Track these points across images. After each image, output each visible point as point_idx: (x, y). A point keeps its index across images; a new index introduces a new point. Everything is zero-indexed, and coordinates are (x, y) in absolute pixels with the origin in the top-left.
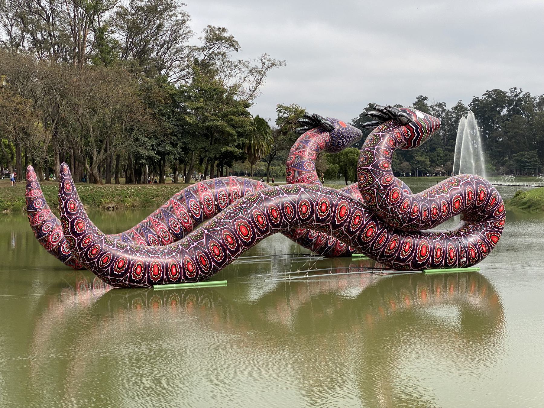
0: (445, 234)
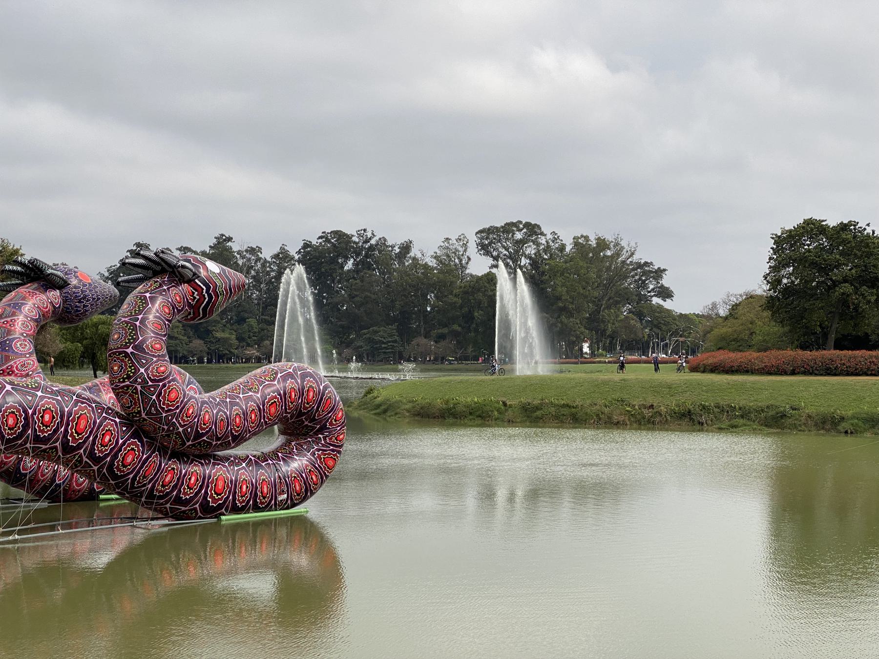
0: (254, 456)
